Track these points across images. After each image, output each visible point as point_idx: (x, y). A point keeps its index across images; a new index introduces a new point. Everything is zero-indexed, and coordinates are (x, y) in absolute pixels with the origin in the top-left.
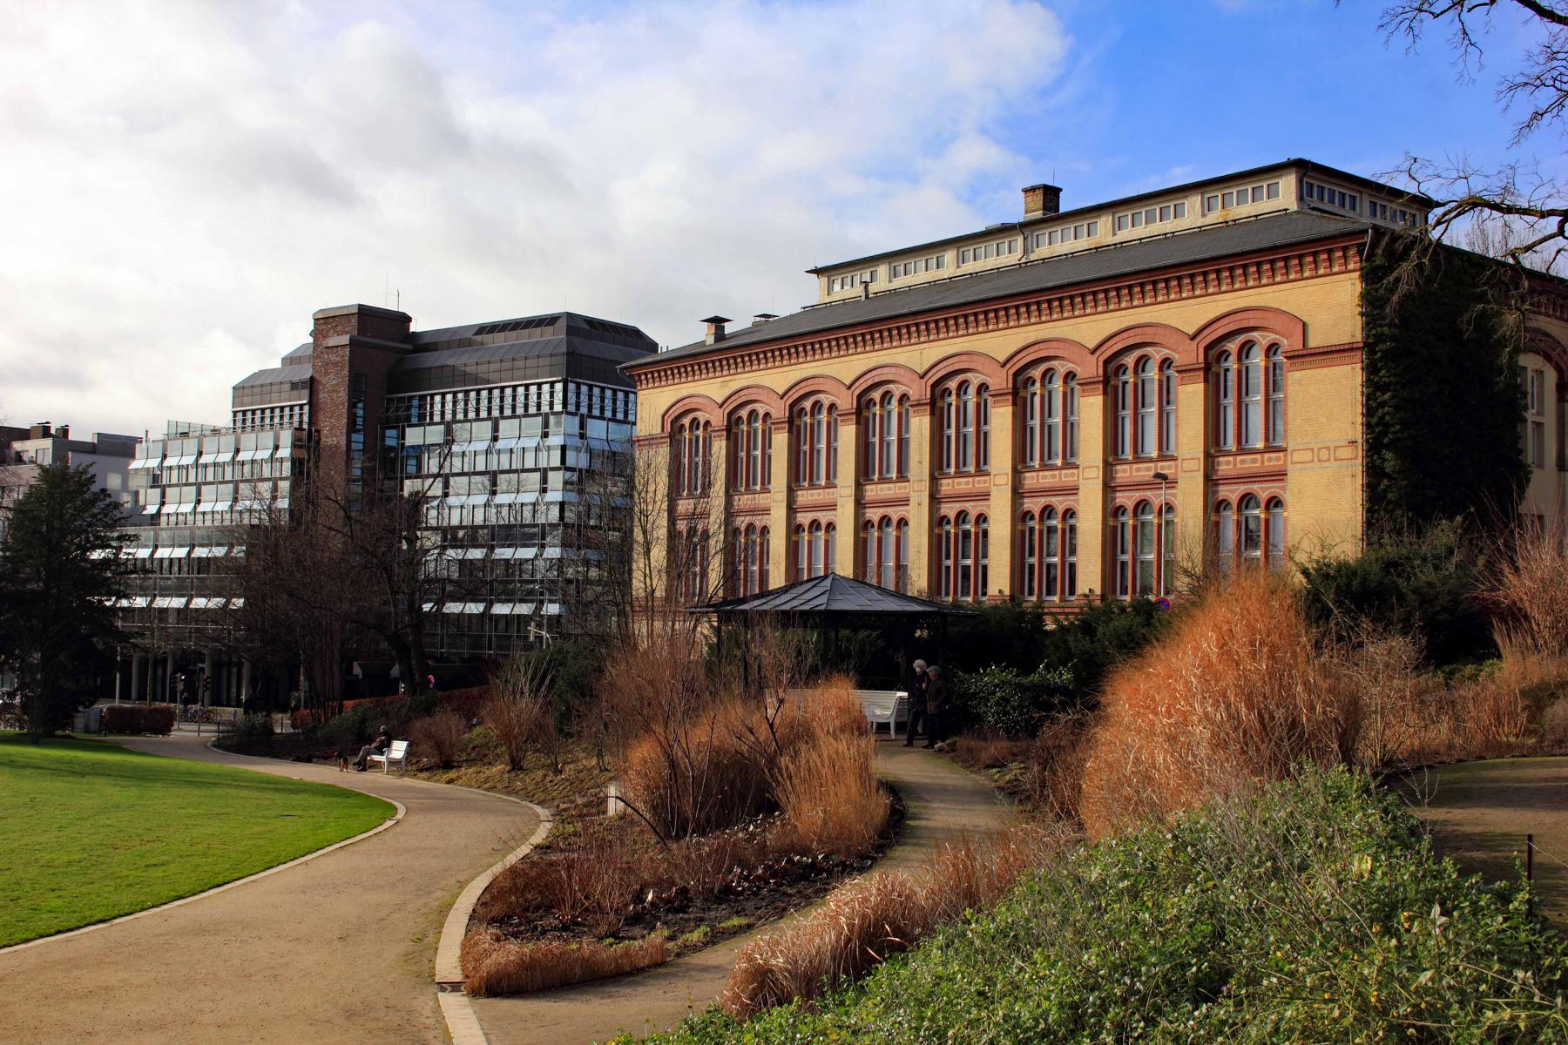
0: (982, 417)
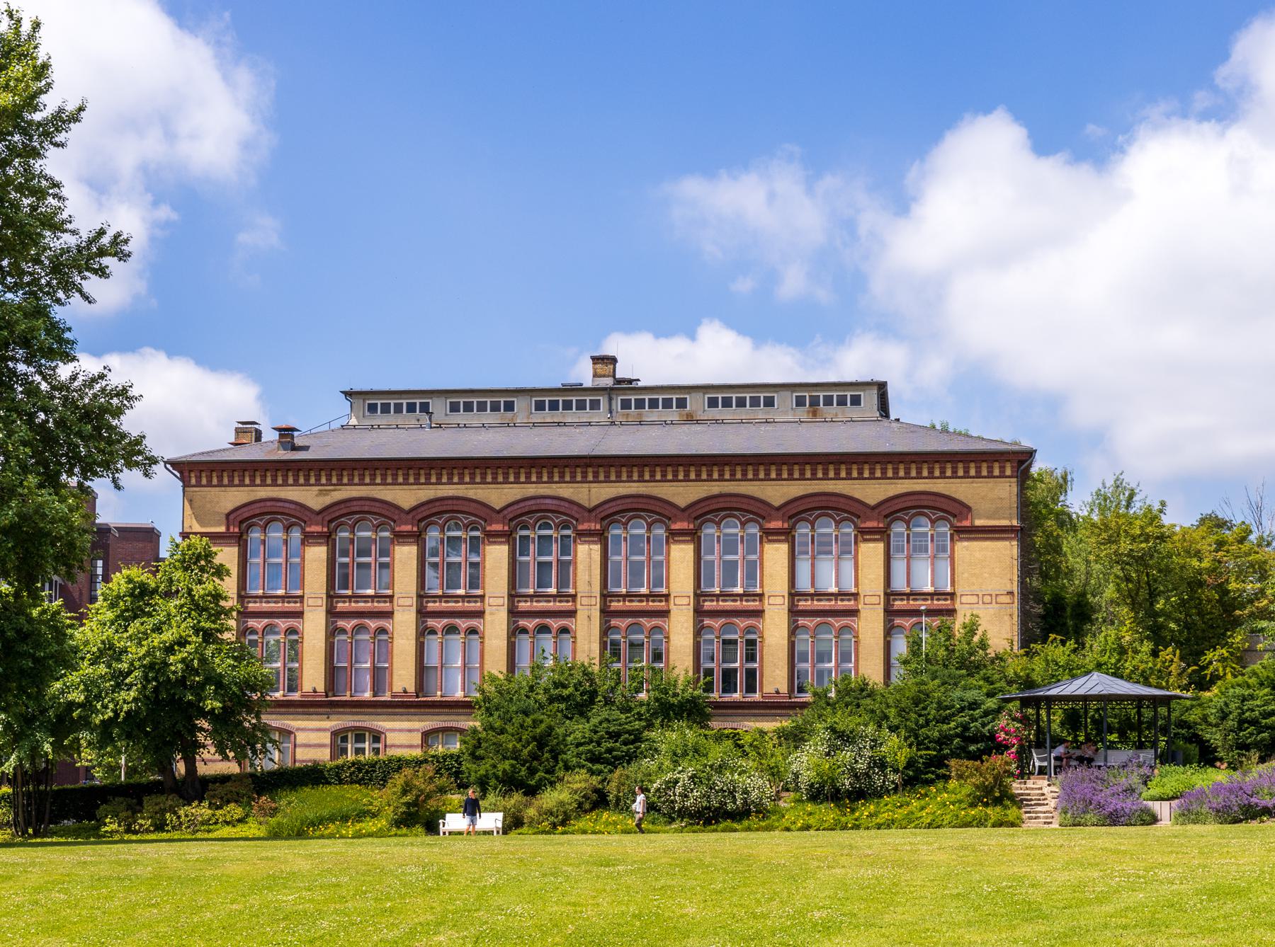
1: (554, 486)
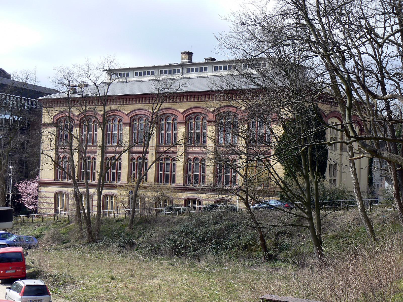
0: (120, 130)
1: (143, 105)
